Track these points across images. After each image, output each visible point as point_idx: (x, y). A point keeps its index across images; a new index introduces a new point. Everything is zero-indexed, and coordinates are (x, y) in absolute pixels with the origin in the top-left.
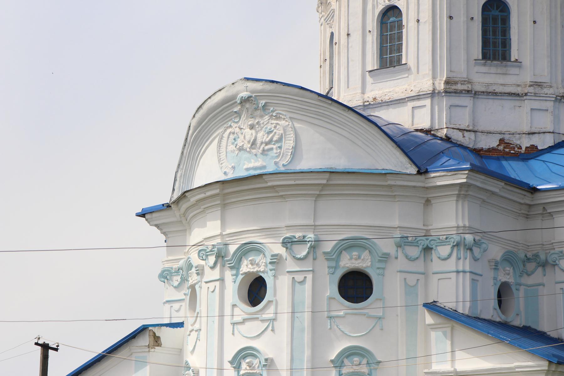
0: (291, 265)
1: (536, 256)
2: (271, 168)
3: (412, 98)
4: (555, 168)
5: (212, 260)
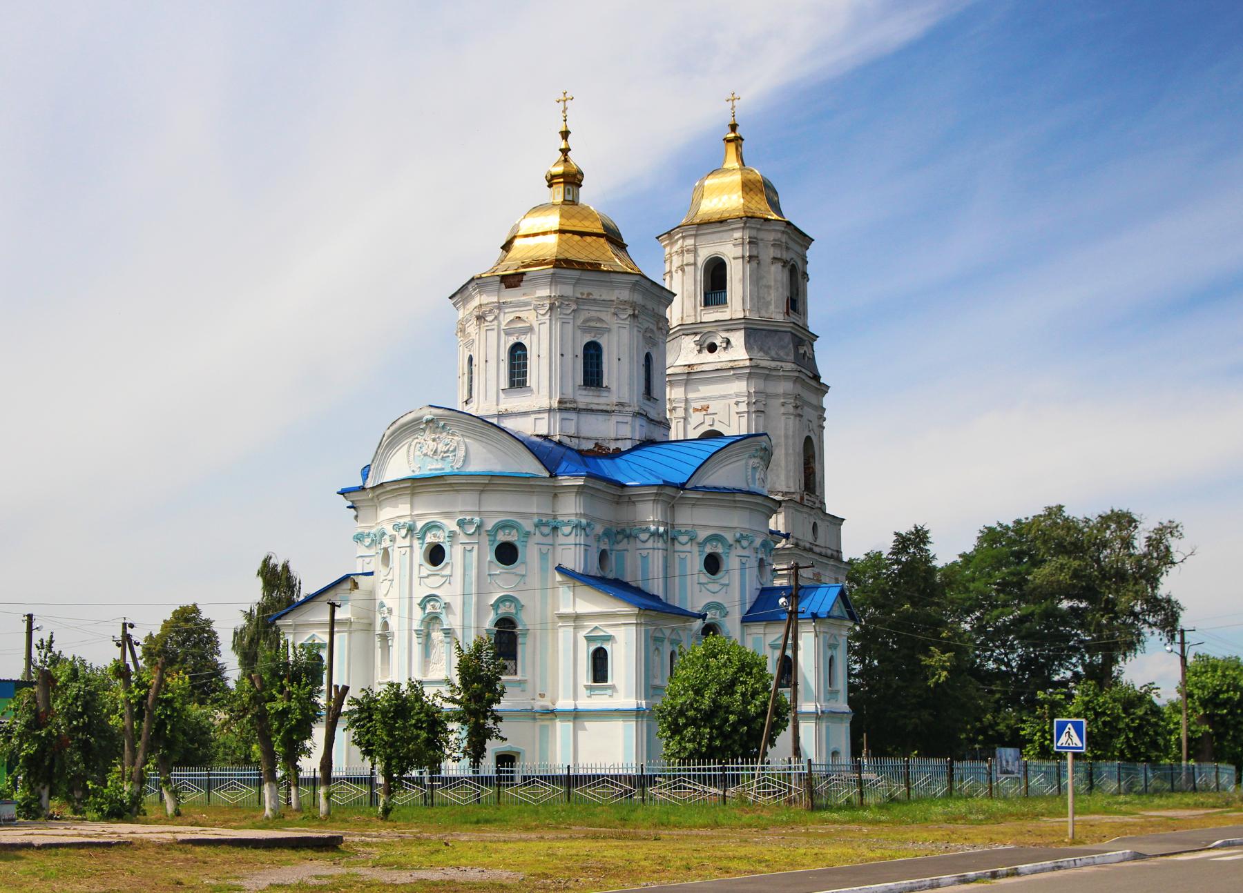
0: (463, 539)
1: (624, 530)
2: (448, 470)
3: (534, 411)
4: (634, 467)
5: (404, 532)
